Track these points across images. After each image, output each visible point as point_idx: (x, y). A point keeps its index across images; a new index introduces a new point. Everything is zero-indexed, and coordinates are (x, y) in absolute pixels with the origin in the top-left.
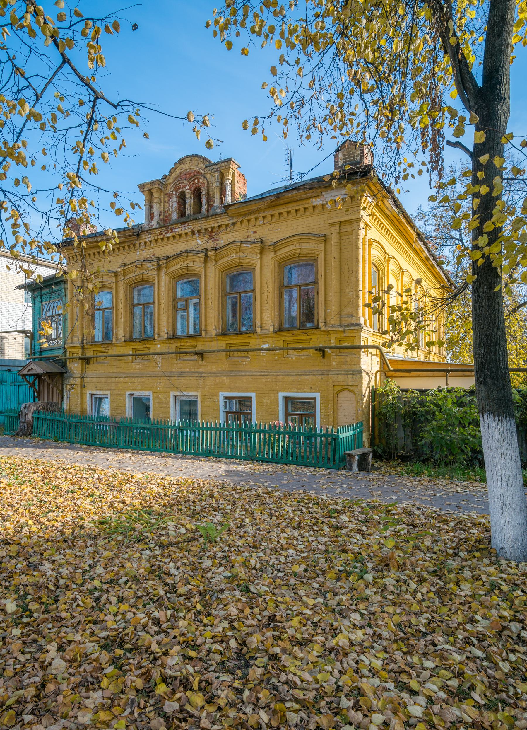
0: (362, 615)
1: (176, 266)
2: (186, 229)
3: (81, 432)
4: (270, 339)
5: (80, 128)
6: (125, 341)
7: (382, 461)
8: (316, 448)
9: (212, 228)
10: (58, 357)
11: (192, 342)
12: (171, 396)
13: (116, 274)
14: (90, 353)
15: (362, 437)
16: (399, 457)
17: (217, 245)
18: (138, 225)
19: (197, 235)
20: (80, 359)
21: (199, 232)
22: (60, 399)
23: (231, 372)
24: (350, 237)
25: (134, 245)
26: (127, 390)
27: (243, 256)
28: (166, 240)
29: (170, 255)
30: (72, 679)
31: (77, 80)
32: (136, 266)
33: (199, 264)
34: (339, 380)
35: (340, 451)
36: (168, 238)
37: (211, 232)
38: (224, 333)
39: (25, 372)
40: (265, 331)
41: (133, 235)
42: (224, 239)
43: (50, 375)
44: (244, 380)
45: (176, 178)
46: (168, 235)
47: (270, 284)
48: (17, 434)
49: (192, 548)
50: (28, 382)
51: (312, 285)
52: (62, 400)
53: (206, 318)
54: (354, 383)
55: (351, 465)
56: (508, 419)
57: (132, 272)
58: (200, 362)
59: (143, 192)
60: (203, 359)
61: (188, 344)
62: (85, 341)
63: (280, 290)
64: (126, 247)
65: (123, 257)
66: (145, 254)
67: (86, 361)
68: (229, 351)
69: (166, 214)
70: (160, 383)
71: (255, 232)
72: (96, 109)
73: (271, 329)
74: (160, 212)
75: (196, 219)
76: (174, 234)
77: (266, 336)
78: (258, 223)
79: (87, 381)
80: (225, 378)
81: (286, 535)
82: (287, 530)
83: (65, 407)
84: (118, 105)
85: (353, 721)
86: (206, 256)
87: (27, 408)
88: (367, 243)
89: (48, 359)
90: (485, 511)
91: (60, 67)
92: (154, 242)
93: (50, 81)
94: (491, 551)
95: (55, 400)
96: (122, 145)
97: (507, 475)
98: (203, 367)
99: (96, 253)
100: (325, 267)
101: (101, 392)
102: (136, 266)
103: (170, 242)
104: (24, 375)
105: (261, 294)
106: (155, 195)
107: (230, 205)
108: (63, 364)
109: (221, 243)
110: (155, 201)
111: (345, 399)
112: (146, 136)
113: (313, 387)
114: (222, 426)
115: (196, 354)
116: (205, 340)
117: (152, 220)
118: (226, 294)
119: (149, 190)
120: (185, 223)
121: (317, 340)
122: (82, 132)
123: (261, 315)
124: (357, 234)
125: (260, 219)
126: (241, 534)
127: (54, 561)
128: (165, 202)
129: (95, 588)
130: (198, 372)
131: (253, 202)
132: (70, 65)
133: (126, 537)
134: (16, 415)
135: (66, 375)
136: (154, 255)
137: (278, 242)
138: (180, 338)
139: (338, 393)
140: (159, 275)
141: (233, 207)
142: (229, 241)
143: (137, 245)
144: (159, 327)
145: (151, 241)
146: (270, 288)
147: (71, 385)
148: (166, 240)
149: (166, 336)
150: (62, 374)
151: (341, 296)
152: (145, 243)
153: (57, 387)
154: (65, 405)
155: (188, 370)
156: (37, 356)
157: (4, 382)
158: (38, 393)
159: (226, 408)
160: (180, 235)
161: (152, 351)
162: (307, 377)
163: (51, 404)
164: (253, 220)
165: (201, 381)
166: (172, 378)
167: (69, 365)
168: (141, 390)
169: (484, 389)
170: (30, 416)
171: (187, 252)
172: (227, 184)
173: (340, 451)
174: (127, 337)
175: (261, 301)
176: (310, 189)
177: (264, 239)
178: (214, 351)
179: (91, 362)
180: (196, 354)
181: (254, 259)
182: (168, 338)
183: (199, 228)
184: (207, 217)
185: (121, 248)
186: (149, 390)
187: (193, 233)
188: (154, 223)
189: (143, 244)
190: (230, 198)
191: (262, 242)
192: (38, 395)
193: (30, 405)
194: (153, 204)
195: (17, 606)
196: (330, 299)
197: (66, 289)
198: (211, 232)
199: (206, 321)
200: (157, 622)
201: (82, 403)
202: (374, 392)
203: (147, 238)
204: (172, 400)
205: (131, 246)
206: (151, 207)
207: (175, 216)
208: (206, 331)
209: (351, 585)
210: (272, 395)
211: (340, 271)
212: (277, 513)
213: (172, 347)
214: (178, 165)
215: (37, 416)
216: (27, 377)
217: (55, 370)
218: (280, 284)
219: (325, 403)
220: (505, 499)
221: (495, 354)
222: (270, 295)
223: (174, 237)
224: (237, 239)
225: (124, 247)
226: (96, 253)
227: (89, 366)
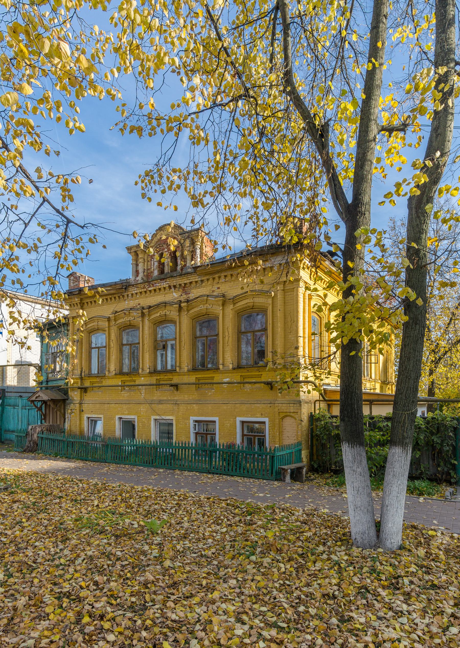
0: (238, 581)
1: (156, 315)
2: (165, 284)
3: (77, 448)
4: (230, 375)
5: (57, 244)
6: (116, 374)
7: (318, 473)
8: (266, 463)
9: (185, 284)
10: (61, 386)
11: (169, 376)
12: (152, 420)
13: (109, 319)
14: (87, 384)
15: (301, 454)
16: (332, 471)
17: (189, 297)
18: (127, 280)
19: (173, 289)
20: (79, 388)
21: (175, 287)
22: (62, 421)
23: (199, 400)
24: (292, 293)
25: (123, 296)
26: (117, 414)
27: (209, 307)
28: (148, 292)
29: (152, 305)
30: (32, 615)
31: (54, 212)
32: (125, 314)
33: (175, 313)
34: (283, 408)
35: (277, 466)
36: (150, 291)
37: (184, 287)
38: (194, 369)
39: (34, 398)
40: (226, 368)
41: (122, 288)
42: (194, 293)
43: (54, 401)
44: (210, 407)
45: (157, 242)
46: (150, 289)
47: (230, 330)
48: (24, 451)
49: (138, 538)
50: (37, 407)
51: (263, 331)
52: (64, 422)
53: (180, 356)
54: (295, 411)
55: (284, 477)
56: (358, 446)
57: (121, 318)
58: (175, 392)
59: (130, 253)
60: (177, 390)
61: (166, 377)
62: (83, 374)
63: (238, 335)
64: (117, 297)
65: (115, 305)
66: (132, 303)
67: (84, 390)
68: (198, 384)
69: (149, 272)
70: (143, 409)
71: (218, 288)
72: (68, 230)
73: (231, 366)
74: (144, 269)
75: (172, 277)
76: (155, 288)
77: (226, 372)
78: (221, 281)
79: (85, 407)
80: (194, 405)
81: (210, 529)
82: (213, 526)
83: (66, 428)
84: (84, 226)
85: (198, 637)
86: (180, 306)
87: (34, 429)
88: (307, 298)
89: (53, 387)
90: (346, 512)
91: (42, 204)
92: (139, 294)
93: (33, 215)
94: (350, 541)
95: (58, 423)
96: (87, 254)
97: (357, 486)
98: (178, 396)
99: (93, 302)
100: (273, 317)
101: (96, 416)
102: (125, 314)
103: (152, 294)
104: (33, 401)
105: (224, 338)
106: (140, 256)
107: (199, 267)
108: (65, 392)
109: (192, 296)
110: (140, 260)
111: (288, 422)
112: (104, 247)
113: (263, 413)
114: (194, 445)
115: (172, 385)
116: (179, 374)
117: (137, 276)
118: (196, 338)
119: (135, 252)
120: (163, 279)
121: (266, 376)
122: (59, 246)
123: (223, 355)
124: (297, 291)
125: (223, 277)
126: (178, 528)
127: (36, 546)
128: (148, 261)
129: (61, 564)
130: (173, 400)
131: (216, 265)
132: (49, 203)
133: (92, 530)
134: (24, 435)
135: (67, 402)
136: (139, 304)
137: (236, 296)
138: (159, 372)
139: (282, 419)
140: (143, 321)
141: (201, 268)
142: (199, 294)
143: (126, 296)
144: (143, 364)
145: (136, 293)
146: (230, 333)
147: (71, 410)
148: (148, 292)
149: (148, 371)
150: (64, 401)
151: (285, 341)
152: (132, 294)
153: (60, 412)
154: (67, 426)
155: (165, 398)
156: (44, 385)
157: (16, 406)
158: (45, 415)
159: (195, 430)
160: (160, 289)
161: (137, 383)
162: (259, 405)
163: (53, 425)
164: (217, 278)
165: (175, 407)
166: (153, 405)
167: (70, 393)
168: (128, 414)
169: (343, 424)
170: (35, 436)
171: (165, 303)
172: (197, 249)
173: (277, 466)
174: (118, 371)
175: (223, 343)
176: (260, 255)
177: (225, 294)
178: (186, 384)
179: (88, 391)
180: (172, 385)
181: (218, 310)
182: (150, 373)
183: (175, 284)
184: (181, 275)
185: (113, 298)
186: (135, 415)
187: (170, 287)
188: (139, 278)
189: (130, 295)
190: (199, 260)
191: (224, 296)
192: (44, 417)
193: (35, 427)
194: (138, 262)
195: (4, 575)
196: (277, 342)
197: (68, 330)
198: (184, 287)
199: (180, 359)
200: (96, 583)
201: (80, 424)
202: (312, 417)
203: (133, 290)
204: (152, 423)
205: (121, 297)
206: (137, 265)
207: (156, 273)
208: (180, 367)
209: (239, 563)
210: (232, 420)
211: (285, 320)
212: (208, 514)
213: (153, 380)
214: (158, 232)
215: (41, 436)
216: (36, 403)
217: (59, 397)
218: (238, 330)
219: (272, 427)
220: (357, 503)
221: (351, 400)
222: (230, 339)
223: (155, 290)
224: (205, 293)
225: (115, 298)
226: (93, 302)
227: (87, 394)
